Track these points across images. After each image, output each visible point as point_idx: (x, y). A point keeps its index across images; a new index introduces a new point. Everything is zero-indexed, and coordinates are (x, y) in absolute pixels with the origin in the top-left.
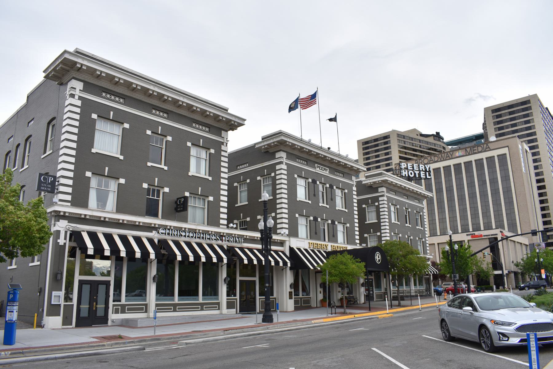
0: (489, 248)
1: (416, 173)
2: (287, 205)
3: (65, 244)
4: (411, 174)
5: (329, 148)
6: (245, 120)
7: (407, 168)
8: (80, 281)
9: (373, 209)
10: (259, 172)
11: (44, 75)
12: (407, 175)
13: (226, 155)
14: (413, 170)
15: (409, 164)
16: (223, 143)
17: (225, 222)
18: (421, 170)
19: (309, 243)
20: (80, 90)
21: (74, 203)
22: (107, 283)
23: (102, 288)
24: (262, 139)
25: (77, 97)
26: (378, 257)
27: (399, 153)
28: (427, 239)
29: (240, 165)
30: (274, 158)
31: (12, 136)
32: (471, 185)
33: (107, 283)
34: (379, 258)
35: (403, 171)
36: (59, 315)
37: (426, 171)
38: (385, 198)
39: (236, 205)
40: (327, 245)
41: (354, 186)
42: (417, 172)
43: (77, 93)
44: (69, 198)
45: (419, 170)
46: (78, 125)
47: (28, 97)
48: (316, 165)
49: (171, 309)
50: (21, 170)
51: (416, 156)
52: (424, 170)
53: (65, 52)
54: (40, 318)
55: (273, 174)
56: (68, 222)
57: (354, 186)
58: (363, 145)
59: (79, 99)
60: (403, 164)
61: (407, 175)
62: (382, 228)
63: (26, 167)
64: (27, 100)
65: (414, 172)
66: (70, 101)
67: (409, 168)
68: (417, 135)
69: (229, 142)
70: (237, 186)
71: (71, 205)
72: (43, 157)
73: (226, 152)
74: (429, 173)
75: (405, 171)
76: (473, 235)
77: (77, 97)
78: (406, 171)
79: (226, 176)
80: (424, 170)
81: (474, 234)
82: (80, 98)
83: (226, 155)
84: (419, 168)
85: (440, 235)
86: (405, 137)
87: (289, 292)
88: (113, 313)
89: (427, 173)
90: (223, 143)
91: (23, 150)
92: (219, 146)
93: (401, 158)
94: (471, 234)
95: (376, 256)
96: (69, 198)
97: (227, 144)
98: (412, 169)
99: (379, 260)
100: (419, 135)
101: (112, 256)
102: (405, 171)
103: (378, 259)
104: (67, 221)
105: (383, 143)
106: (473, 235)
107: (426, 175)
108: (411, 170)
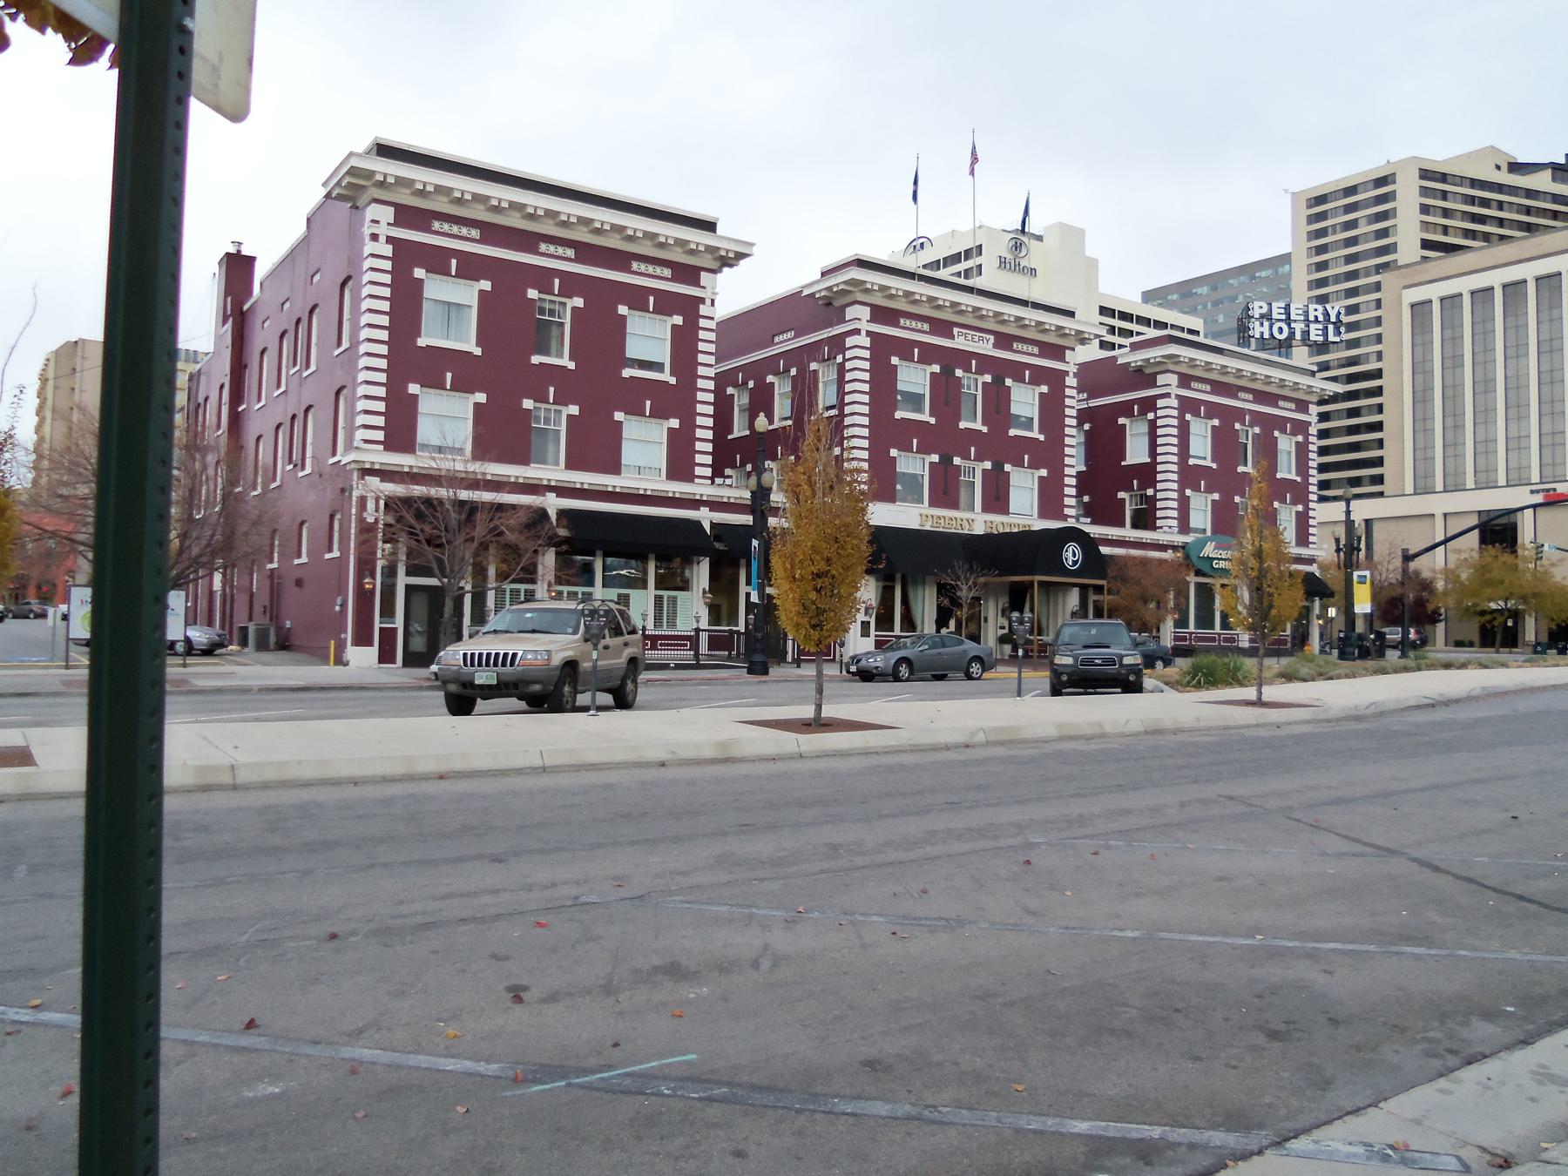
0: (1476, 532)
3: (377, 520)
4: (1281, 330)
5: (1388, 162)
6: (752, 245)
7: (1267, 316)
8: (409, 588)
9: (1143, 428)
10: (812, 351)
11: (324, 192)
12: (1266, 336)
13: (712, 325)
14: (1288, 321)
15: (1274, 305)
16: (702, 300)
17: (708, 472)
18: (1312, 318)
19: (921, 515)
20: (388, 224)
21: (390, 444)
24: (823, 274)
25: (382, 239)
26: (1071, 555)
27: (1421, 231)
28: (1312, 505)
29: (784, 332)
30: (842, 320)
31: (288, 300)
32: (1453, 361)
34: (1074, 555)
35: (1257, 323)
38: (1175, 403)
39: (729, 437)
40: (973, 520)
41: (1071, 374)
42: (1299, 327)
43: (384, 231)
44: (380, 436)
45: (1307, 320)
47: (308, 219)
48: (956, 330)
49: (686, 645)
50: (305, 374)
51: (1487, 237)
52: (1321, 318)
53: (351, 154)
54: (341, 647)
55: (839, 359)
57: (1071, 374)
58: (1309, 207)
60: (1257, 304)
61: (1266, 336)
62: (1159, 477)
63: (313, 368)
64: (308, 227)
65: (1289, 325)
66: (370, 247)
67: (1275, 316)
68: (1498, 167)
69: (718, 296)
70: (733, 395)
71: (385, 449)
72: (337, 352)
73: (712, 318)
74: (1335, 328)
75: (1262, 324)
76: (1552, 492)
77: (382, 239)
78: (1266, 324)
79: (711, 372)
80: (1321, 318)
81: (1555, 490)
82: (389, 240)
83: (712, 325)
85: (1442, 490)
86: (1448, 177)
87: (862, 622)
89: (1331, 327)
90: (702, 300)
91: (306, 328)
92: (690, 308)
93: (1426, 244)
94: (1543, 490)
95: (1067, 551)
96: (380, 436)
97: (713, 301)
98: (1283, 317)
99: (1075, 563)
100: (1505, 167)
102: (1262, 324)
103: (1071, 558)
106: (1552, 492)
107: (1325, 334)
108: (1279, 320)
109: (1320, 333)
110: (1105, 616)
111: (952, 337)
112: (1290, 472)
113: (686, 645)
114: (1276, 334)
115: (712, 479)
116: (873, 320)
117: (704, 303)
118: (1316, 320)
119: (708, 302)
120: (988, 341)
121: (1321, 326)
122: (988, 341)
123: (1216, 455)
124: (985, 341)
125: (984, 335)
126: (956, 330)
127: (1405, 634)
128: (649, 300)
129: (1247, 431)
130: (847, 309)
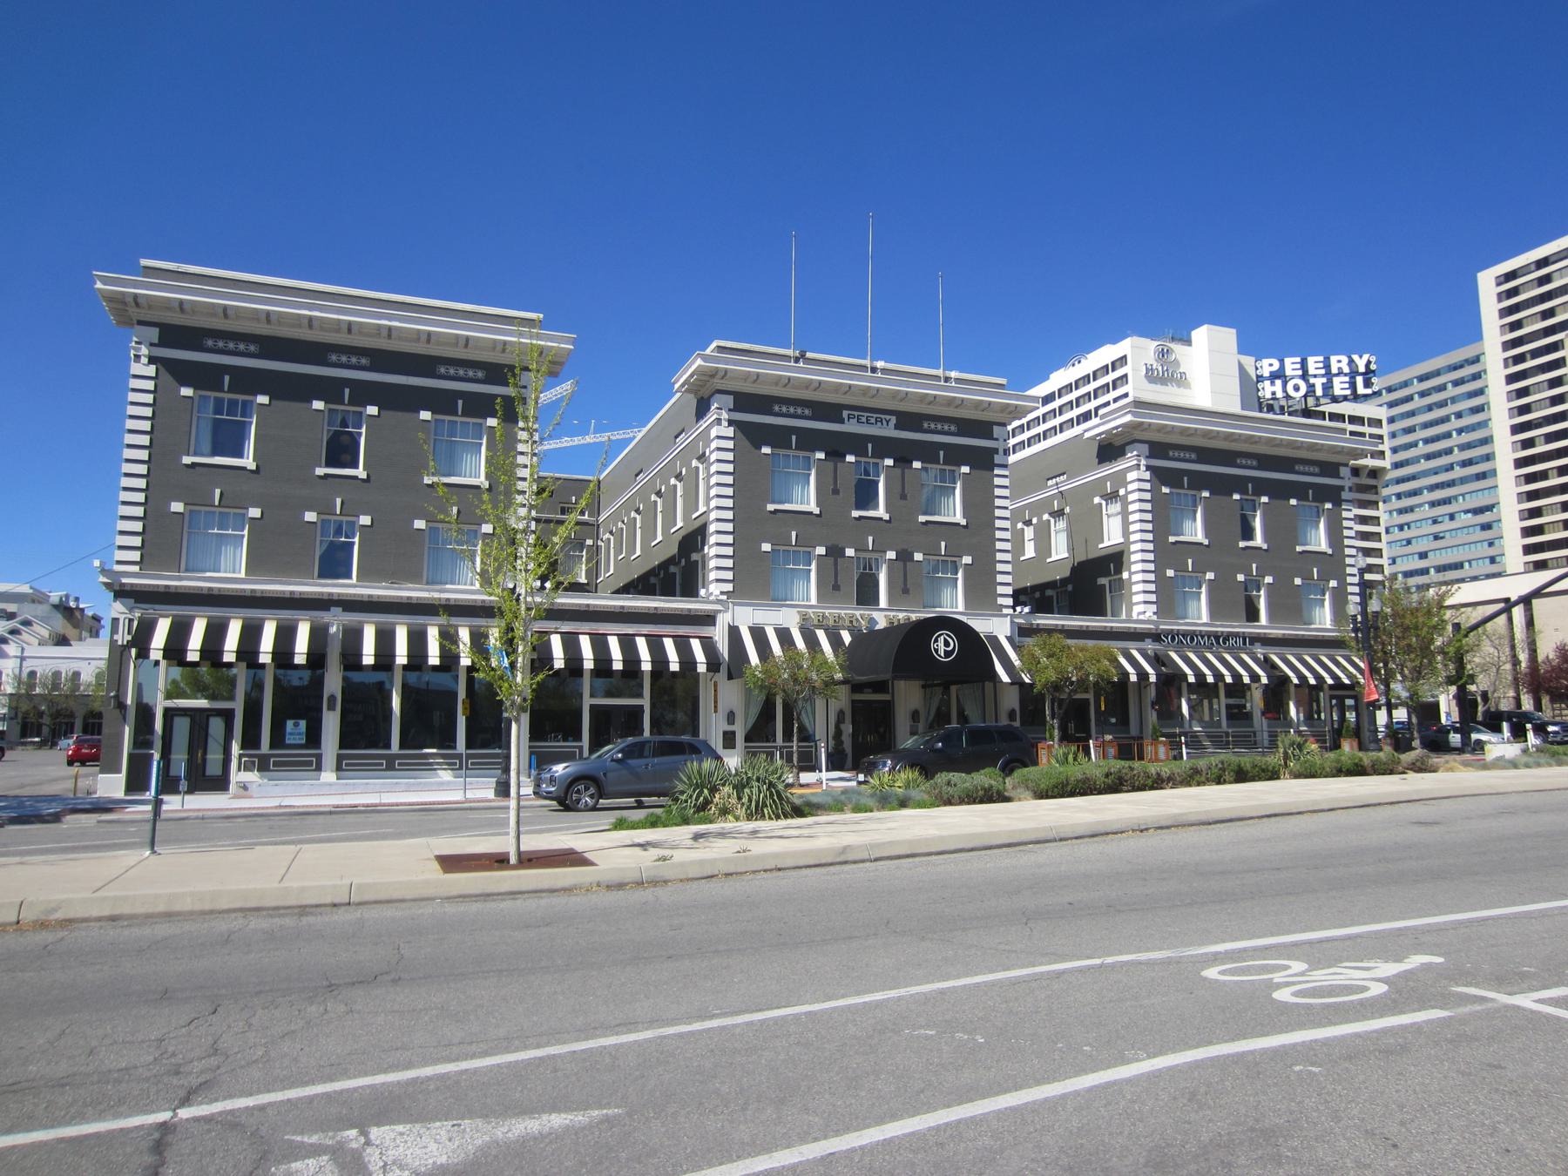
1: (1313, 385)
2: (1349, 591)
4: (1297, 388)
14: (1305, 376)
16: (996, 451)
17: (1010, 601)
18: (1334, 370)
20: (730, 410)
22: (228, 716)
23: (216, 726)
25: (144, 360)
33: (228, 716)
34: (947, 644)
36: (118, 771)
37: (1354, 373)
42: (1318, 383)
46: (1346, 549)
49: (382, 764)
52: (1346, 370)
56: (135, 602)
58: (1499, 284)
59: (730, 425)
61: (1280, 394)
65: (1307, 381)
67: (1289, 372)
78: (1278, 382)
84: (1327, 366)
88: (239, 770)
90: (996, 451)
95: (936, 641)
99: (948, 654)
101: (240, 663)
104: (133, 600)
105: (1546, 384)
109: (1347, 386)
110: (1232, 701)
111: (842, 421)
112: (808, 503)
113: (382, 764)
114: (1291, 392)
115: (1014, 608)
116: (736, 409)
117: (997, 453)
118: (1340, 373)
119: (1001, 451)
120: (888, 422)
121: (1347, 379)
122: (888, 422)
123: (1331, 545)
124: (884, 422)
125: (883, 416)
126: (845, 413)
127: (1350, 707)
128: (457, 403)
129: (1317, 507)
130: (1127, 448)
